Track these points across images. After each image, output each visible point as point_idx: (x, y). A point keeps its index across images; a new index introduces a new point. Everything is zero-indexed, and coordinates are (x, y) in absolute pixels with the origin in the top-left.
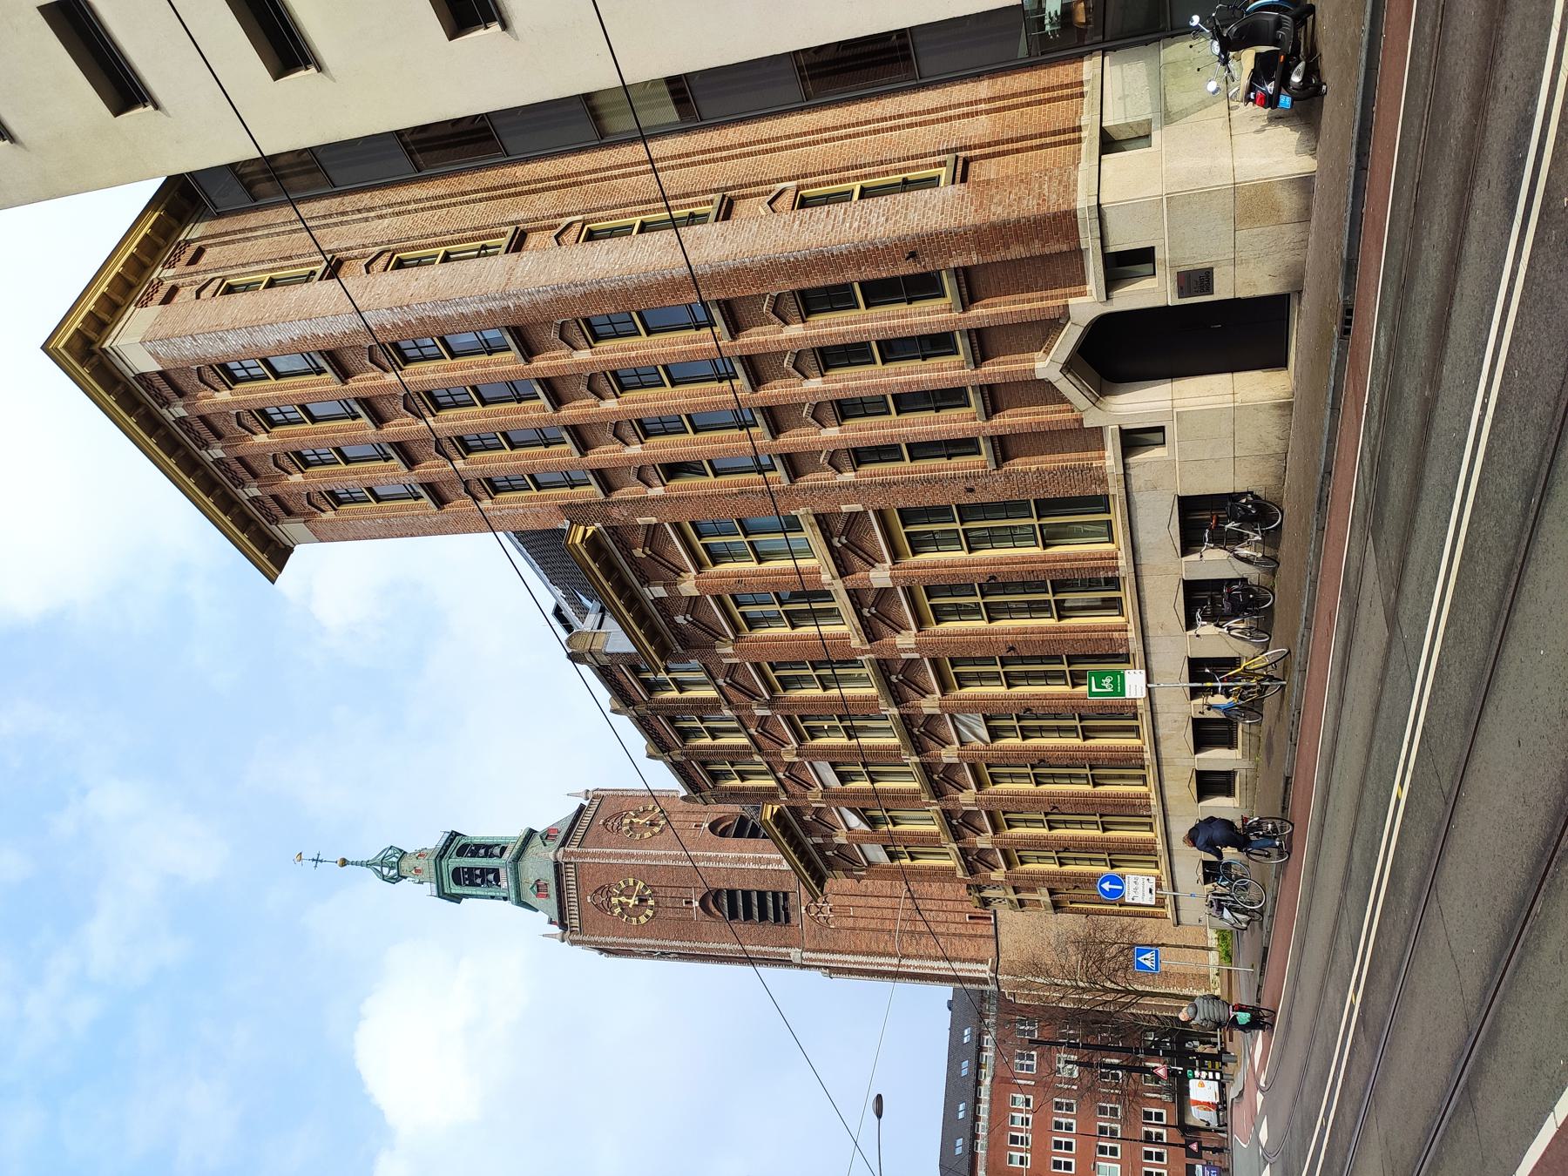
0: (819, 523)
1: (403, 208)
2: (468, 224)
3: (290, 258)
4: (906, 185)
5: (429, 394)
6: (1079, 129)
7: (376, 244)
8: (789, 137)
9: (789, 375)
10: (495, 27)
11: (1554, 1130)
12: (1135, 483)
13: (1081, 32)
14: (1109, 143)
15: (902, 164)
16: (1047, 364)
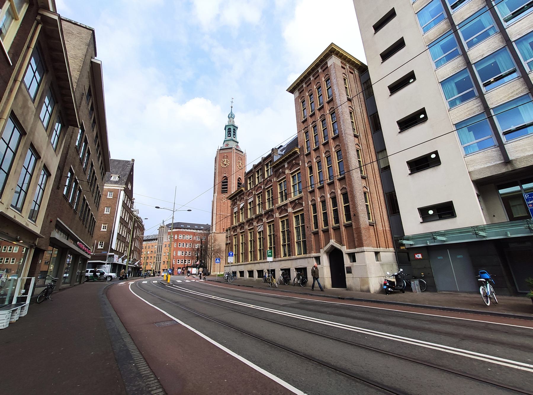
0: (301, 197)
1: (362, 113)
2: (359, 126)
3: (351, 91)
4: (368, 214)
5: (325, 119)
6: (380, 247)
7: (355, 108)
8: (378, 190)
9: (330, 191)
10: (399, 131)
11: (193, 330)
12: (309, 259)
13: (399, 248)
14: (377, 253)
15: (373, 213)
16: (333, 242)
